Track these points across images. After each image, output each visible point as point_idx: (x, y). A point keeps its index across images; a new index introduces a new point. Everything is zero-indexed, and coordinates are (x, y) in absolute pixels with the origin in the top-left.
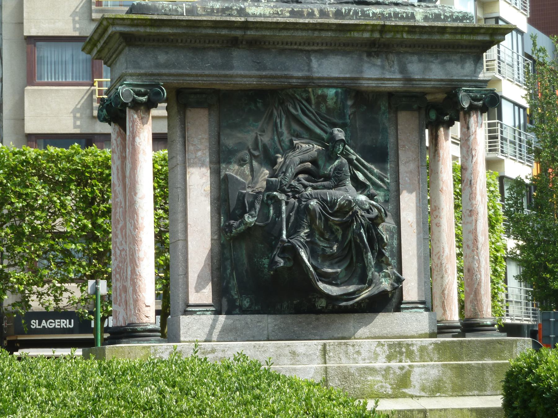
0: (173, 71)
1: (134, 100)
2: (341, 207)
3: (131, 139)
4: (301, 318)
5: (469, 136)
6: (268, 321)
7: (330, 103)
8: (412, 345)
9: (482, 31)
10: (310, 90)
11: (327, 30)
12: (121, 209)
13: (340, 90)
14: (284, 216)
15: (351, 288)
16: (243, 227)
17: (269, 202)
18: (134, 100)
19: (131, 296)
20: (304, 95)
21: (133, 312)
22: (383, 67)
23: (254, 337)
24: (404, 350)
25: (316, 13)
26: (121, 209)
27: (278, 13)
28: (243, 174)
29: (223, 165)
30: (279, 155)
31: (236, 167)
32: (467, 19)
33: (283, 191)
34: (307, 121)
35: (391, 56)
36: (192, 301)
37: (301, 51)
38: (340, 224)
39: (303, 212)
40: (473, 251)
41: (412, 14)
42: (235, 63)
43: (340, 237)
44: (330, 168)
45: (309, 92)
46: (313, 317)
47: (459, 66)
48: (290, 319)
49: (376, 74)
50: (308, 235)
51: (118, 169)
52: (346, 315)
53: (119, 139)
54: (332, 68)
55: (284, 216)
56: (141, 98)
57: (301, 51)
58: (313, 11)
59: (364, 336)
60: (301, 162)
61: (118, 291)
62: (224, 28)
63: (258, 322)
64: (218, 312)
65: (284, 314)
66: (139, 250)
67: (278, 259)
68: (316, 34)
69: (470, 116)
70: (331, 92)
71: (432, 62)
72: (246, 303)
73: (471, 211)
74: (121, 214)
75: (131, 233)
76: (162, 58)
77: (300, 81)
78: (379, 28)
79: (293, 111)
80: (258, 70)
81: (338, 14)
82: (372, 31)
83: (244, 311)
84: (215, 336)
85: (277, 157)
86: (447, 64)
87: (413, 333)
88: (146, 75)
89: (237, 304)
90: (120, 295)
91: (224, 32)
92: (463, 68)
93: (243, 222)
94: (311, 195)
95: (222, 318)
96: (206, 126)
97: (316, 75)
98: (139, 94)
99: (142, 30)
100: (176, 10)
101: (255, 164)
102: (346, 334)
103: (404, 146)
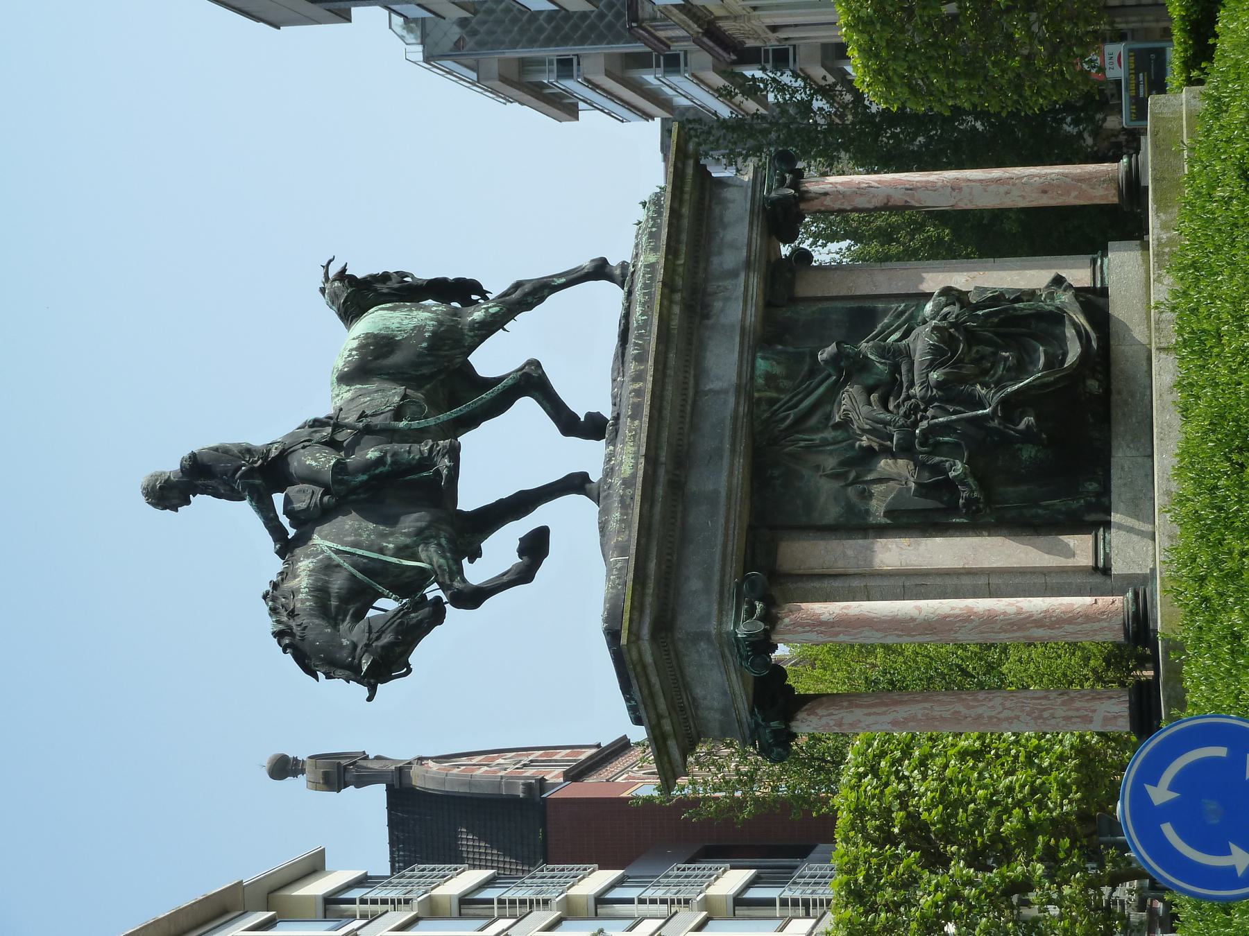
0: (717, 567)
1: (761, 619)
2: (941, 340)
3: (823, 629)
4: (1116, 413)
5: (838, 192)
6: (1122, 458)
7: (778, 370)
8: (1159, 239)
9: (680, 165)
10: (756, 395)
11: (666, 358)
12: (936, 708)
13: (759, 354)
14: (954, 417)
15: (1070, 332)
16: (970, 481)
17: (931, 441)
18: (761, 619)
19: (1079, 628)
20: (764, 407)
21: (1105, 624)
22: (727, 299)
23: (1147, 475)
24: (1167, 250)
25: (637, 386)
26: (936, 708)
27: (634, 436)
28: (885, 494)
29: (871, 520)
30: (857, 444)
31: (874, 502)
32: (659, 199)
33: (915, 424)
34: (807, 403)
35: (710, 289)
36: (1089, 562)
37: (695, 402)
38: (969, 345)
39: (949, 393)
40: (1014, 185)
41: (646, 266)
42: (710, 487)
43: (989, 349)
44: (881, 367)
45: (760, 399)
46: (1115, 398)
47: (731, 205)
48: (1118, 428)
49: (737, 305)
50: (984, 385)
51: (870, 714)
52: (1113, 356)
53: (820, 712)
54: (724, 363)
55: (954, 417)
56: (758, 610)
57: (695, 402)
58: (634, 390)
59: (1147, 333)
60: (870, 404)
61: (1070, 713)
62: (653, 490)
63: (1123, 469)
64: (1107, 525)
65: (1110, 437)
66: (1005, 613)
67: (1022, 426)
68: (670, 372)
69: (807, 192)
70: (762, 365)
71: (722, 239)
72: (1093, 486)
73: (953, 189)
74: (943, 708)
75: (976, 627)
76: (695, 584)
77: (742, 402)
78: (666, 291)
79: (788, 422)
80: (721, 457)
81: (640, 359)
82: (671, 302)
83: (1106, 490)
84: (1147, 527)
85: (860, 446)
86: (726, 220)
87: (1142, 270)
88: (721, 603)
89: (1093, 500)
90: (1078, 710)
91: (660, 491)
92: (733, 202)
93: (961, 480)
94: (922, 383)
95: (1115, 517)
96: (805, 544)
97: (734, 379)
98: (751, 612)
99: (649, 600)
100: (620, 569)
101: (869, 477)
102: (1144, 356)
103: (849, 288)
